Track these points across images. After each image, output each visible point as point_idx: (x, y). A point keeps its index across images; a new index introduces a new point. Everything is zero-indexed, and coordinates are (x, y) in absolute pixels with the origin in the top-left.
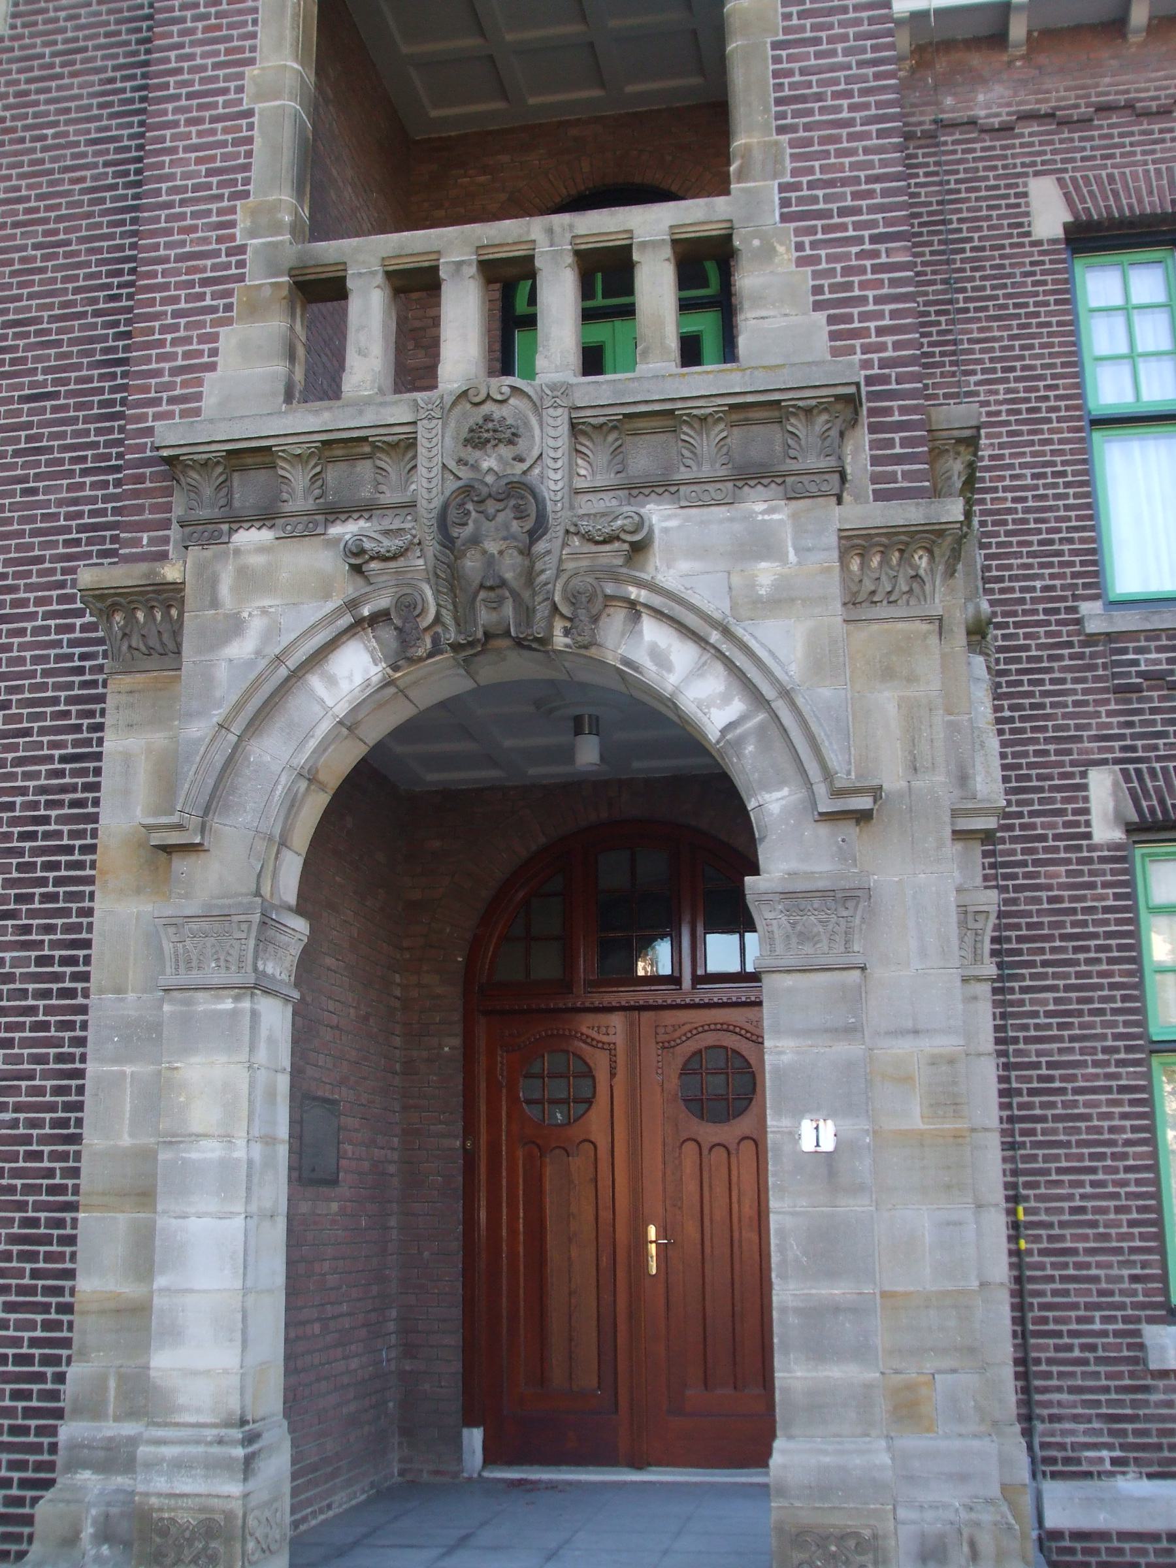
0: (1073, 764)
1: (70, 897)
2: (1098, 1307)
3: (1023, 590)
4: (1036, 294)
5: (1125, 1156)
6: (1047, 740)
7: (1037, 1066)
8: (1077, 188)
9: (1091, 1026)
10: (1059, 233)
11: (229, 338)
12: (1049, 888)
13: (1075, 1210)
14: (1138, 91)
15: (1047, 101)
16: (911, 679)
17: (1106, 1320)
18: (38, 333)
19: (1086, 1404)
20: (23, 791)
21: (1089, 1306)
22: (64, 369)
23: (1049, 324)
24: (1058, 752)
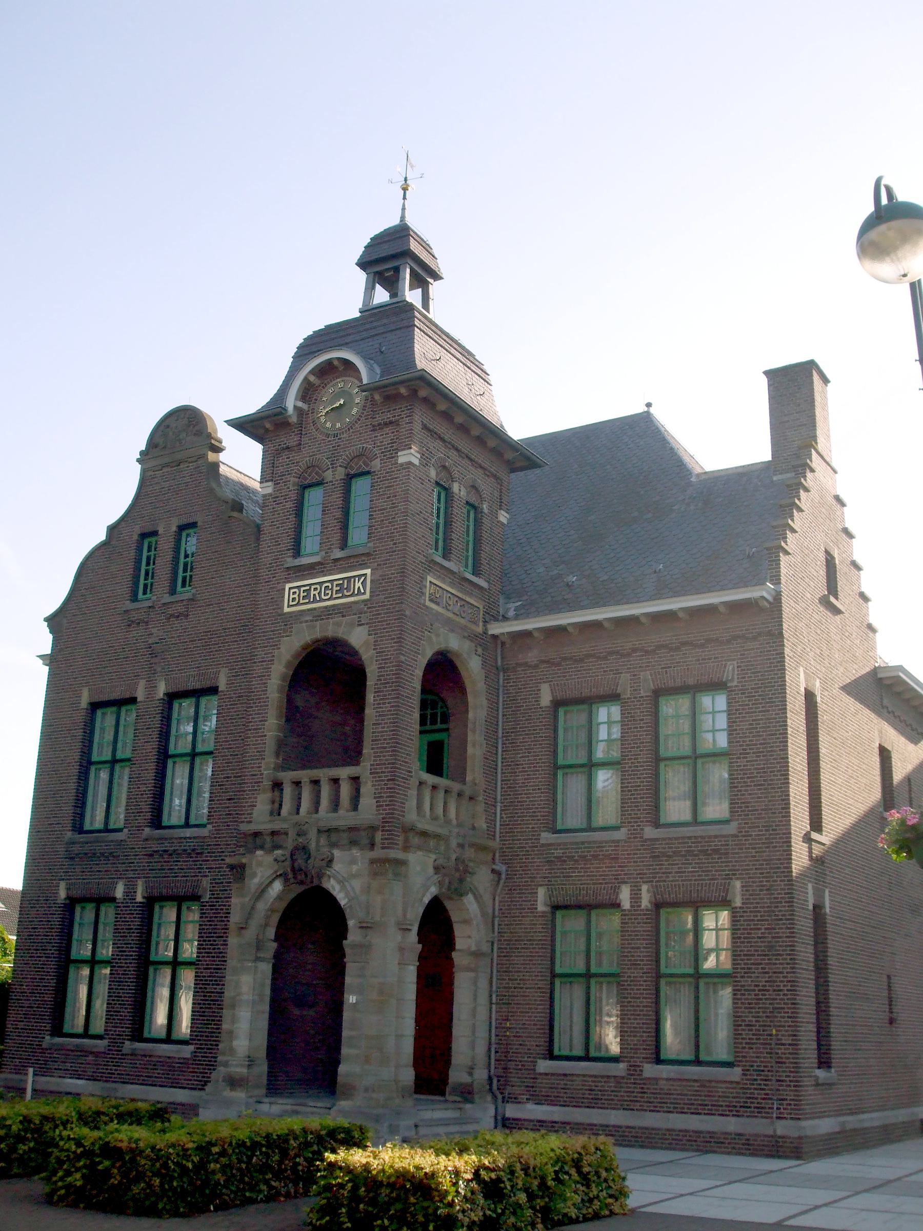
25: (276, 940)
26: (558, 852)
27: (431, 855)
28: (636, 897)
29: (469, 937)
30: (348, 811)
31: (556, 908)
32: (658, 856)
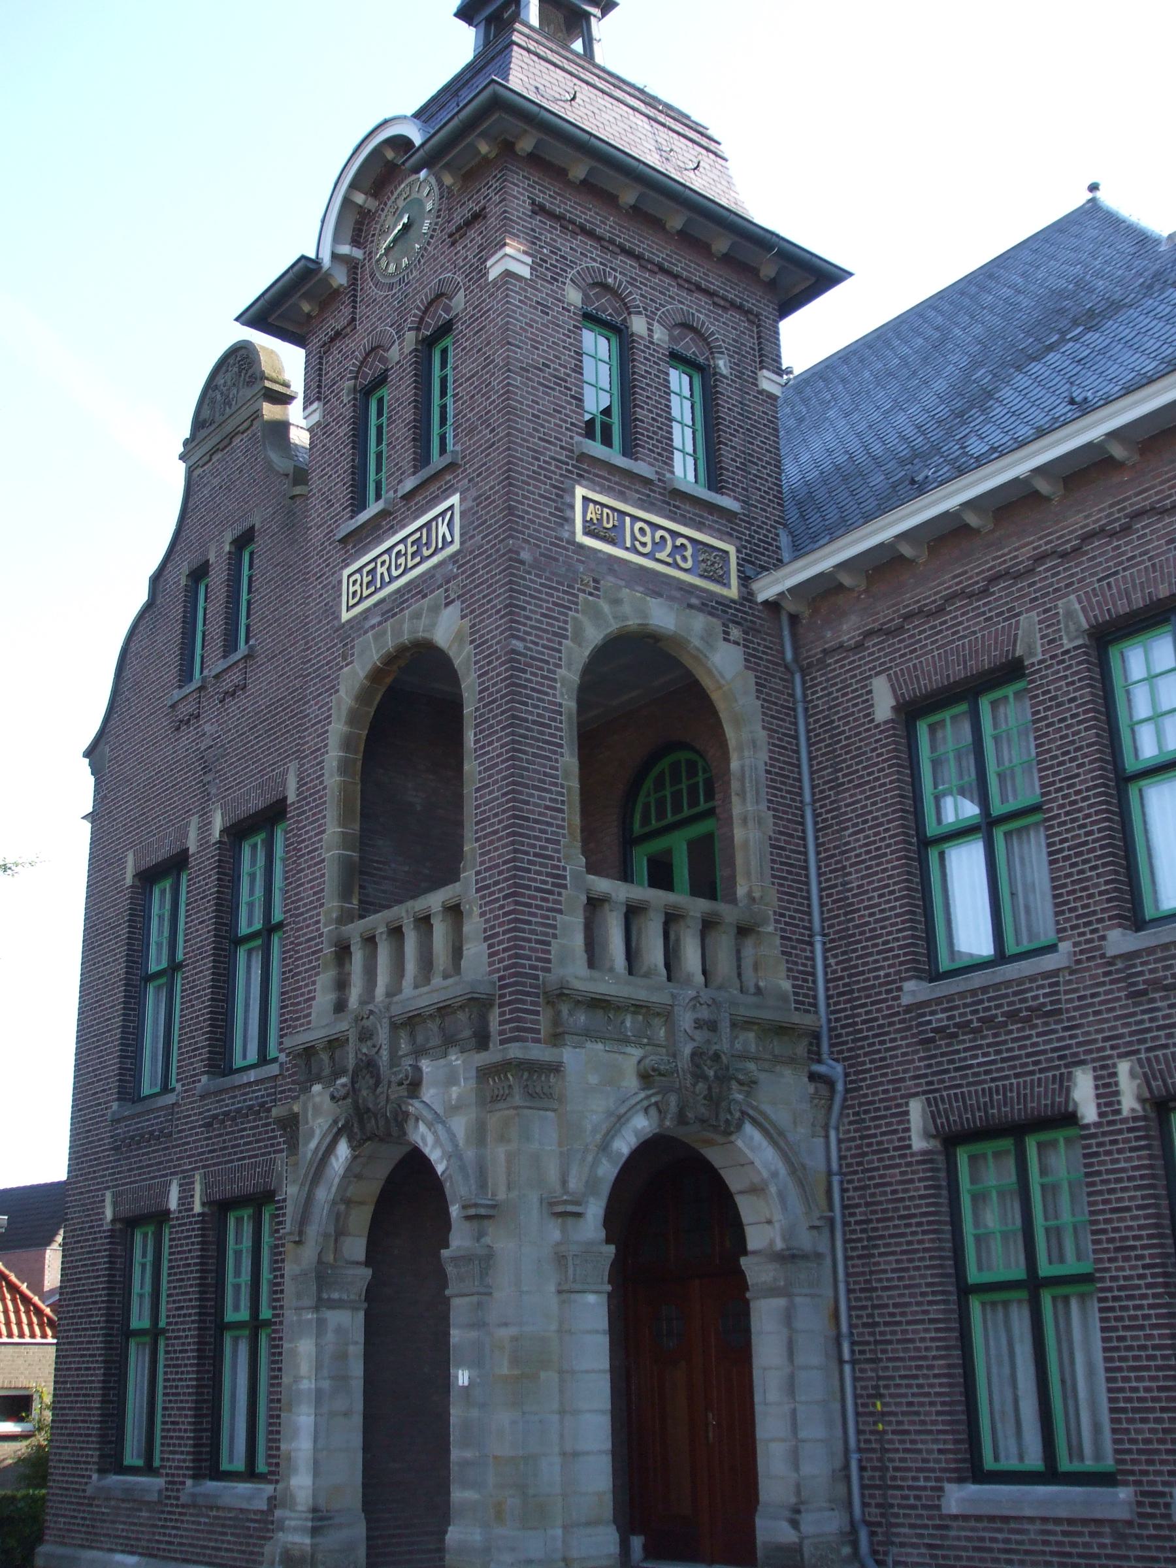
14: (925, 598)
16: (509, 1141)
25: (368, 1262)
26: (939, 1019)
27: (629, 1050)
28: (1107, 1092)
29: (769, 1222)
31: (951, 1140)
32: (1144, 993)
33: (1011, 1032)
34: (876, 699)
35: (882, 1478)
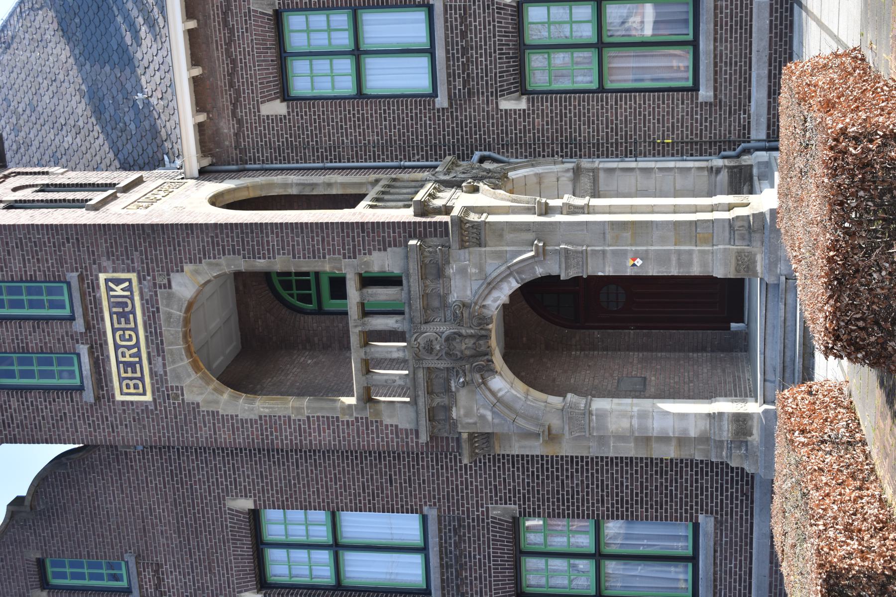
0: (497, 114)
1: (557, 463)
2: (692, 116)
3: (430, 128)
4: (310, 115)
5: (640, 104)
6: (488, 123)
7: (607, 133)
8: (266, 97)
9: (593, 113)
10: (285, 104)
11: (387, 421)
12: (543, 125)
13: (658, 122)
14: (224, 71)
15: (227, 106)
17: (696, 114)
18: (368, 482)
19: (725, 122)
20: (523, 479)
21: (692, 119)
22: (381, 473)
23: (323, 111)
24: (493, 119)
30: (402, 290)
31: (522, 89)
33: (471, 38)
34: (272, 113)
35: (696, 143)
